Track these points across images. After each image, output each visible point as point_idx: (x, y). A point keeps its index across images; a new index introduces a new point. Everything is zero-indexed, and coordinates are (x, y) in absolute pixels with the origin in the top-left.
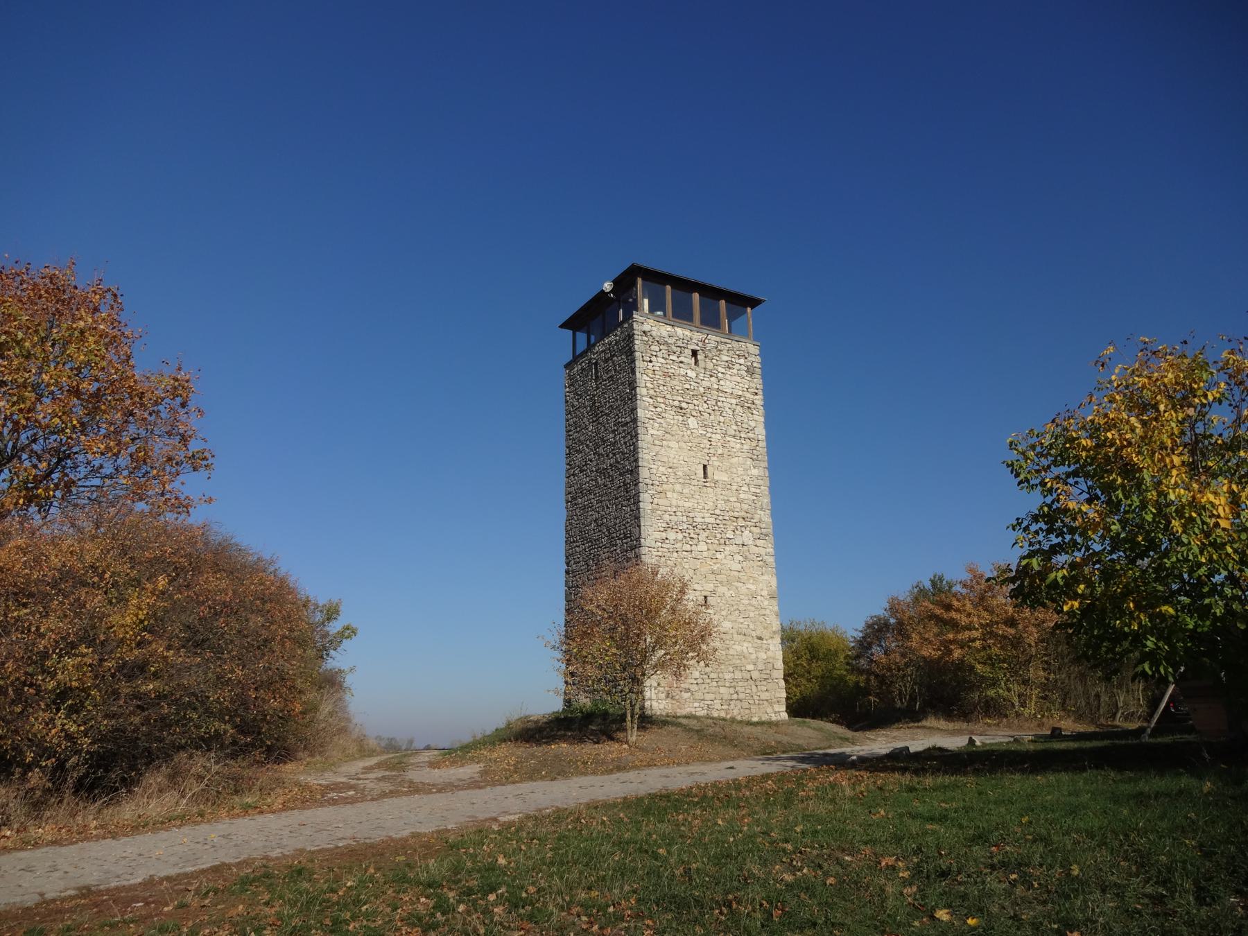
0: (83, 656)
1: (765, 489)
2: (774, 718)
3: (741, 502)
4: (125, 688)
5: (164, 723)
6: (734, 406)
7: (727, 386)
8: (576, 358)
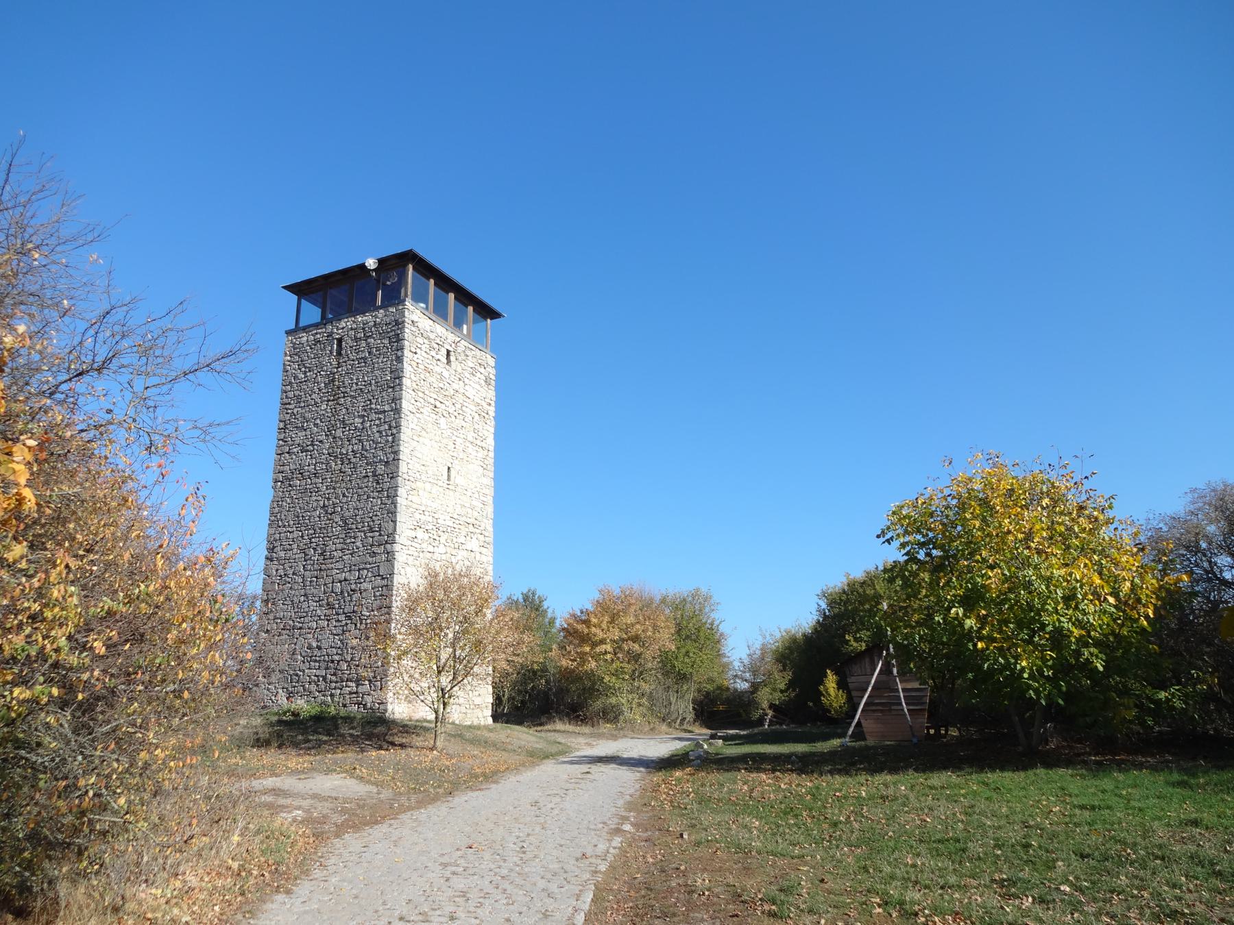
1: (490, 500)
7: (471, 392)
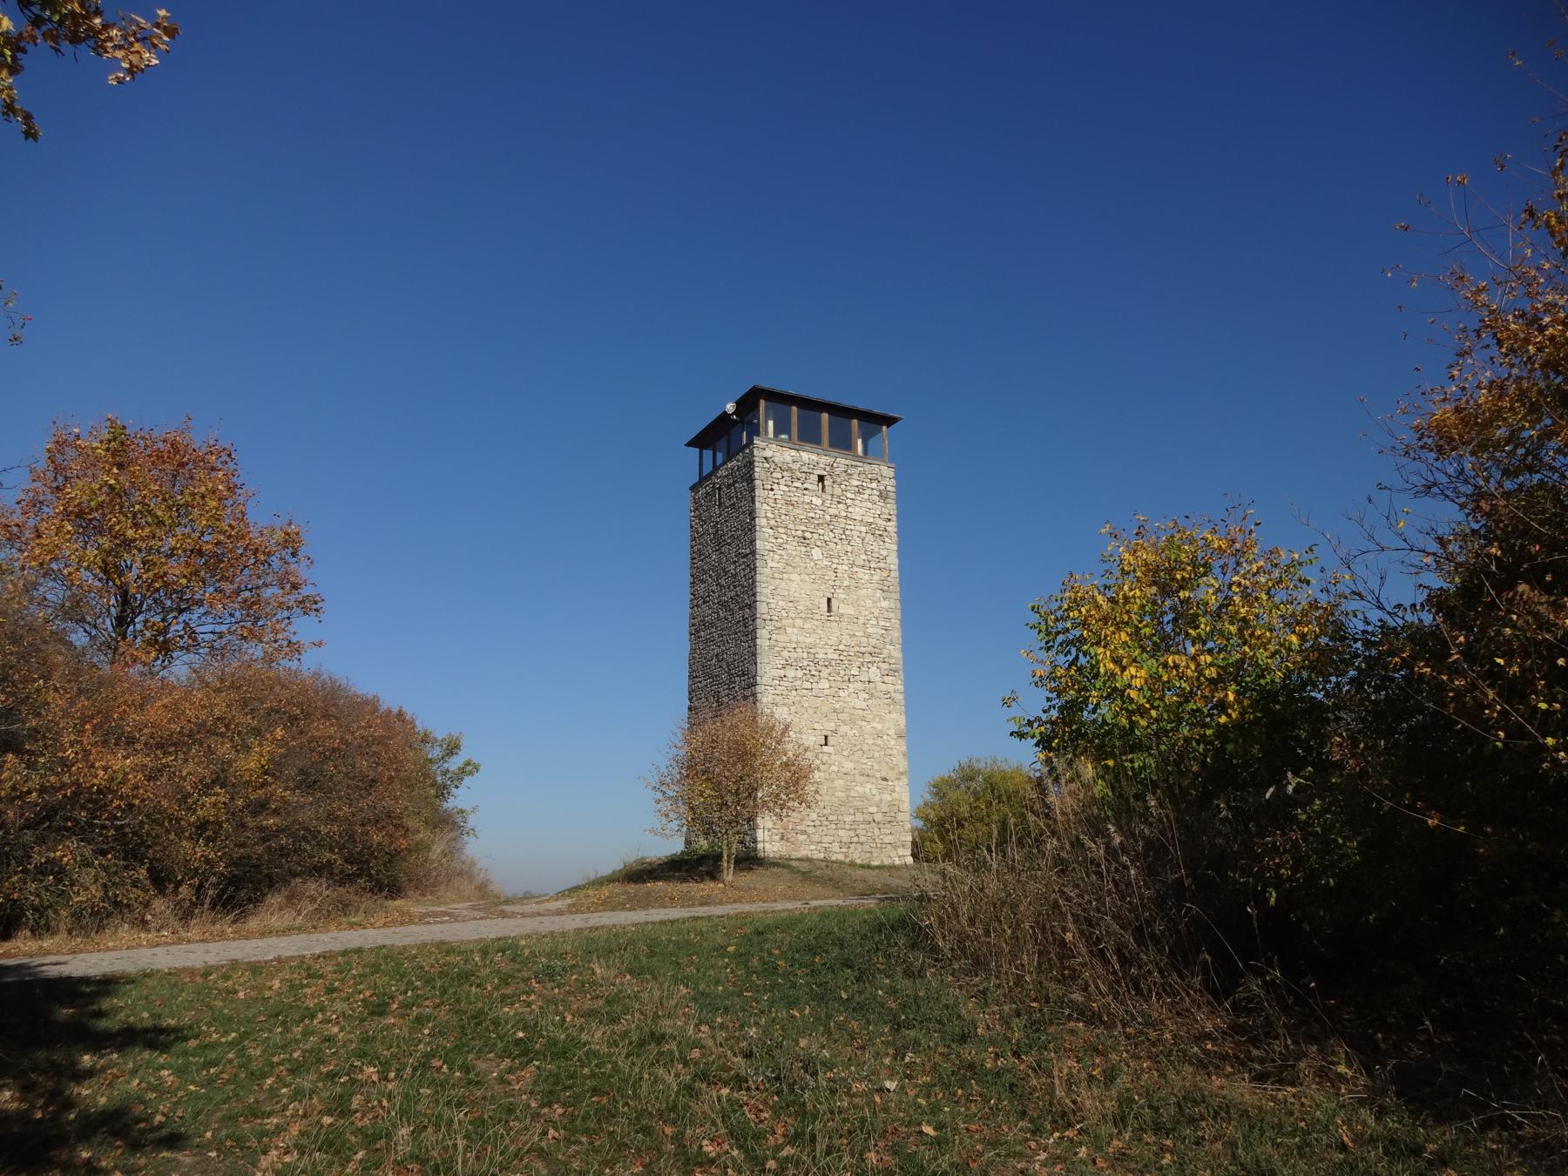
0: (218, 794)
1: (896, 622)
2: (897, 862)
3: (868, 636)
4: (250, 822)
5: (283, 852)
6: (863, 534)
7: (856, 512)
8: (703, 479)
